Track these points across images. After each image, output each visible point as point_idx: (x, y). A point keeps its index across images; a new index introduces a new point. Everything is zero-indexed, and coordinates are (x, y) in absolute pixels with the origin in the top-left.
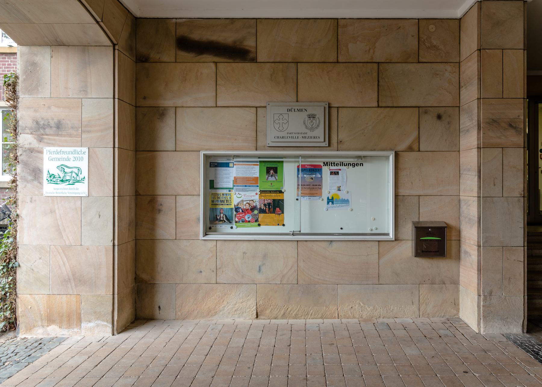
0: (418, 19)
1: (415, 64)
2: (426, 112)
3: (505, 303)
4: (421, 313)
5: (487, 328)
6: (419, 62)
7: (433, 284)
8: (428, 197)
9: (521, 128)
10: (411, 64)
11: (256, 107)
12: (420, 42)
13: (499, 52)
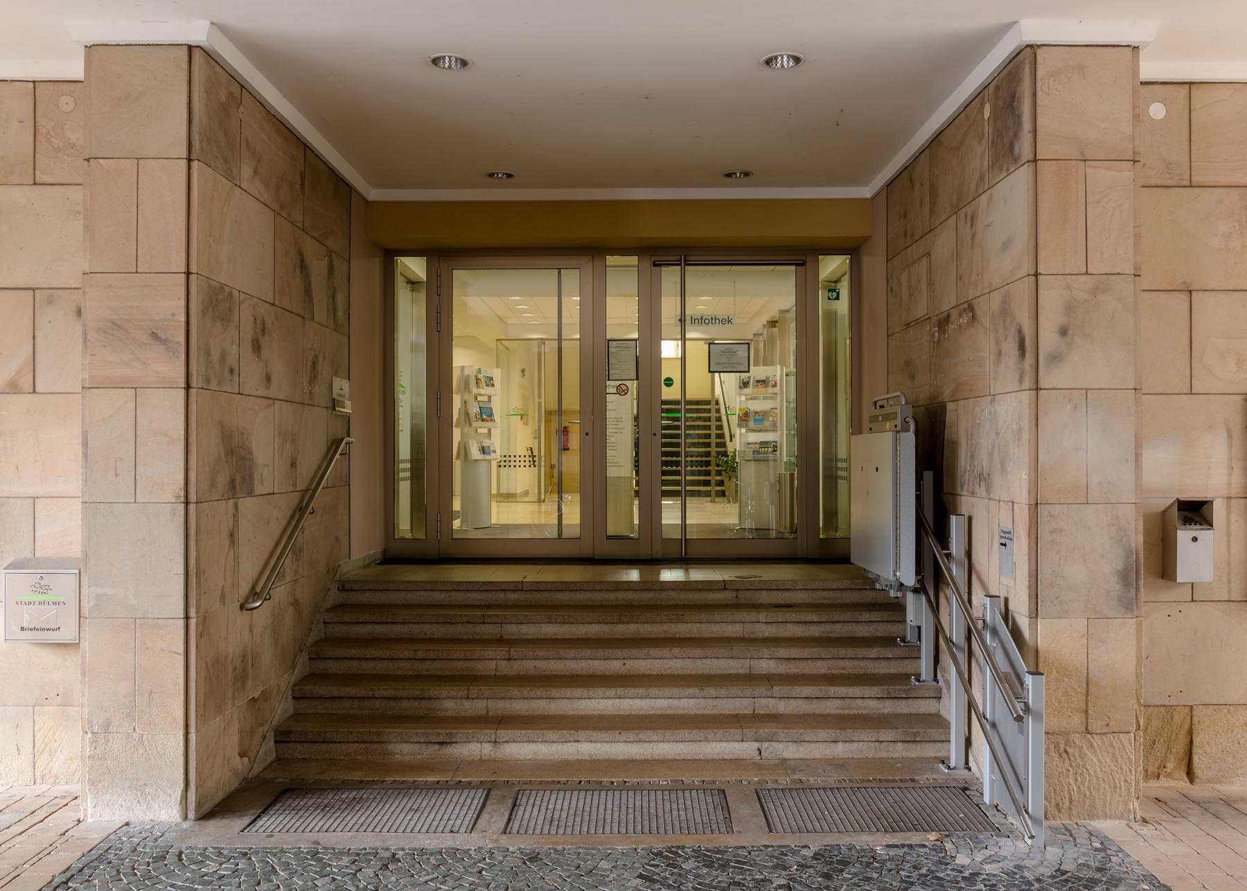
0: (34, 82)
1: (27, 188)
2: (51, 302)
3: (141, 751)
4: (38, 774)
5: (98, 808)
6: (35, 184)
7: (65, 705)
8: (55, 500)
9: (178, 343)
10: (17, 189)
11: (1087, 274)
12: (38, 136)
13: (129, 165)
